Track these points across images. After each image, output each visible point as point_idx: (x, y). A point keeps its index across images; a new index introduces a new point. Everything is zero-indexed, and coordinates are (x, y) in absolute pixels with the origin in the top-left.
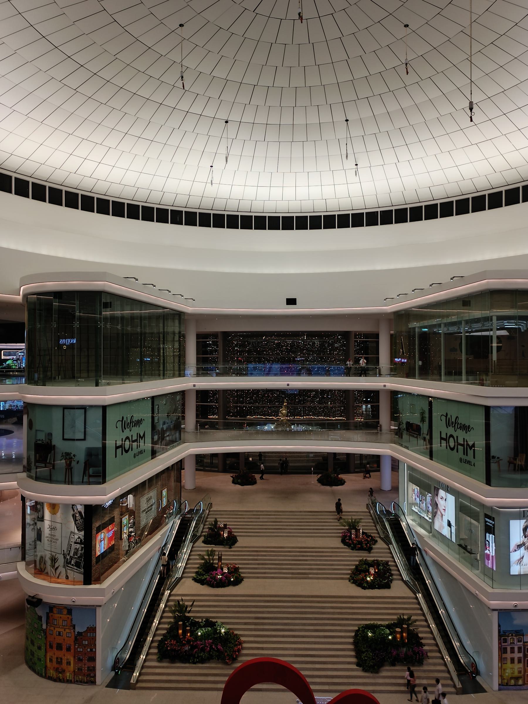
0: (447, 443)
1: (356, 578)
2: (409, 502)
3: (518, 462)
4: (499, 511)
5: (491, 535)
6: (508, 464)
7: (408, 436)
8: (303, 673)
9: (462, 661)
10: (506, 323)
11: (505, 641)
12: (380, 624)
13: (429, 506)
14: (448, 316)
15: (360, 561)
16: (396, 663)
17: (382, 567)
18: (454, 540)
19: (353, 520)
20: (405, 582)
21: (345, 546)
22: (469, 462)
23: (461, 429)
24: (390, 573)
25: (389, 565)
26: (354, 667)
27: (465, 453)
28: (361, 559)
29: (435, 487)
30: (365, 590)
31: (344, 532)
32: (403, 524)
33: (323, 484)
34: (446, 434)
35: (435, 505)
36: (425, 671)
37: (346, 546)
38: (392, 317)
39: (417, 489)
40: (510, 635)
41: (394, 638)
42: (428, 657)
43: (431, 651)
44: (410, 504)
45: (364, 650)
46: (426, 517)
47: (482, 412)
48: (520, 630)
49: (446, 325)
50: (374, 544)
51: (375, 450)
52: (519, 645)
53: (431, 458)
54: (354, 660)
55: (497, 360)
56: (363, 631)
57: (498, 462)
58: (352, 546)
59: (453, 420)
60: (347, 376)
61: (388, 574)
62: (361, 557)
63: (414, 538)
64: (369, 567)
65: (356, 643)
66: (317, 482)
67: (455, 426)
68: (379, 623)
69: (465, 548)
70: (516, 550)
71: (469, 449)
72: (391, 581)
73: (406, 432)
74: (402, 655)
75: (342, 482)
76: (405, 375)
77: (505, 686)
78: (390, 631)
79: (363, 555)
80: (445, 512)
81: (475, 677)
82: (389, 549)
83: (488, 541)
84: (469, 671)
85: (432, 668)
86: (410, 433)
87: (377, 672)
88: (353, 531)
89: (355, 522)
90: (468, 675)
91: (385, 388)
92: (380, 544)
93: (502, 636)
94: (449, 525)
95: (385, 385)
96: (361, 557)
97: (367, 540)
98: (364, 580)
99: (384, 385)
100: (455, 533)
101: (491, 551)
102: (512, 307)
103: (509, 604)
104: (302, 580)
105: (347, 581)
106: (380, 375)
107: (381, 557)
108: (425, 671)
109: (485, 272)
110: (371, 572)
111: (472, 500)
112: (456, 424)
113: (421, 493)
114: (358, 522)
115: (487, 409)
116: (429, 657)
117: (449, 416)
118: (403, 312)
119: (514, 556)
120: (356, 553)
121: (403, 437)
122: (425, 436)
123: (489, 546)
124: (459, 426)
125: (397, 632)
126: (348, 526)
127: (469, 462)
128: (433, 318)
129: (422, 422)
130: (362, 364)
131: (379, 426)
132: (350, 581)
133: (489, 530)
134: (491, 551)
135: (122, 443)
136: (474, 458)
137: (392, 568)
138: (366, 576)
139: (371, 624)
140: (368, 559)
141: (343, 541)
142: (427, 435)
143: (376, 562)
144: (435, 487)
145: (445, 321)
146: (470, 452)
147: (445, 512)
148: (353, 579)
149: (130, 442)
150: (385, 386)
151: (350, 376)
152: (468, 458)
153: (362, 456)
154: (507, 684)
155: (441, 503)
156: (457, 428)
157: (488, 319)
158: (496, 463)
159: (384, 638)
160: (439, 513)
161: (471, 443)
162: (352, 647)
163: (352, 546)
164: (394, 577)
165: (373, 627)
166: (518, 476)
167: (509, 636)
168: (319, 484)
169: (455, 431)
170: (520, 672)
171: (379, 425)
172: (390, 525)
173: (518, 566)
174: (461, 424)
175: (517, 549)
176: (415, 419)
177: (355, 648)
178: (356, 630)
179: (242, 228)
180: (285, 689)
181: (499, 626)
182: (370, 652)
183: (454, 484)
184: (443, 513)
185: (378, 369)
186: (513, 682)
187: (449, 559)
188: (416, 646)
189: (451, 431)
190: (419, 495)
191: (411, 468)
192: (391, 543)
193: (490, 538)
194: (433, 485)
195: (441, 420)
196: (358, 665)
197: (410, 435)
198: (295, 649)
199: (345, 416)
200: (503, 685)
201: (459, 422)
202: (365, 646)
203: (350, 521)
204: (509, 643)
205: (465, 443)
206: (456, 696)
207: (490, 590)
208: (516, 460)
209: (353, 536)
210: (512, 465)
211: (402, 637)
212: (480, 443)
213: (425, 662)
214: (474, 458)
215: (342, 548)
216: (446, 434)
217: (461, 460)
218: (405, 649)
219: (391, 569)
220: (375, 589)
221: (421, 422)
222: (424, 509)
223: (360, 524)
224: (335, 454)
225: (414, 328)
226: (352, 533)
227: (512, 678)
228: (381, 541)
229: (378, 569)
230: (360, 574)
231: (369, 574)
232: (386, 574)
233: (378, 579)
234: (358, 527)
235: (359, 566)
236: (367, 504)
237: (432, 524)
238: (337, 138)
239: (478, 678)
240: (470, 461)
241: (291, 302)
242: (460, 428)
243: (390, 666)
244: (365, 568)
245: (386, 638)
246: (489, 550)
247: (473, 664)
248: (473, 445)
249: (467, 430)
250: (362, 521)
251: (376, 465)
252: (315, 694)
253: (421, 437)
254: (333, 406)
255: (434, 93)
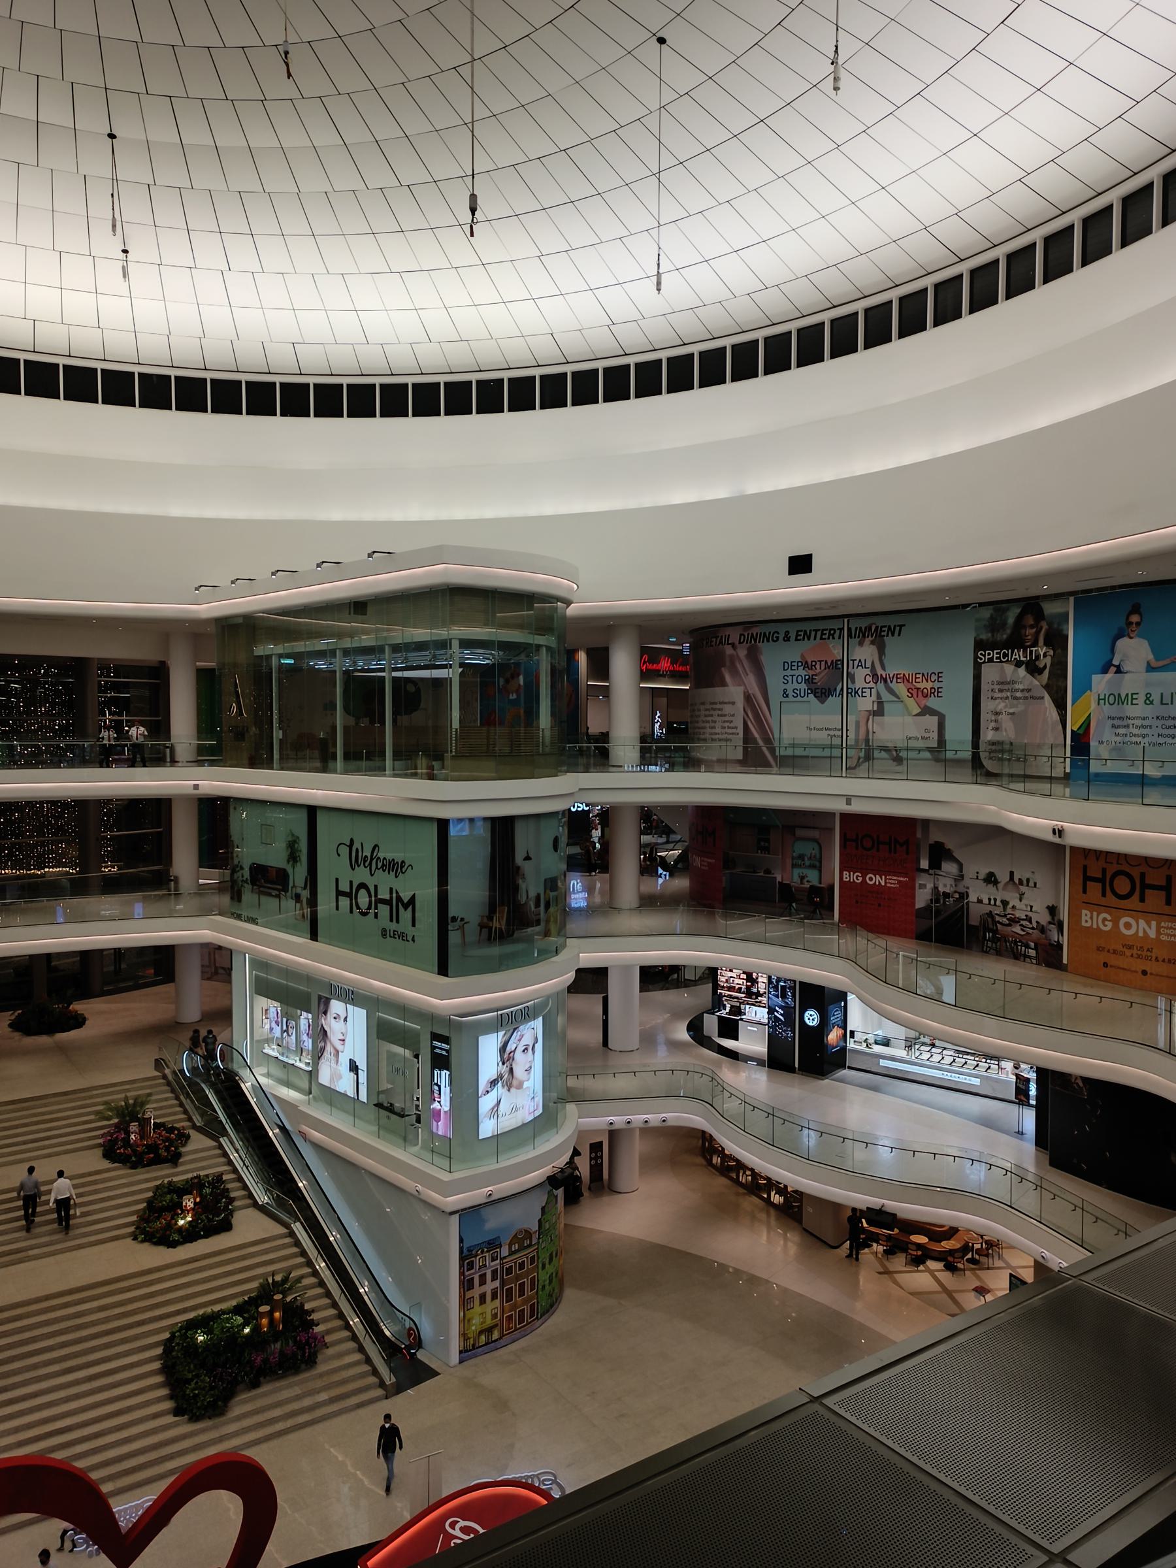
0: (351, 900)
1: (150, 1228)
2: (256, 1038)
3: (495, 924)
4: (461, 1021)
5: (443, 1072)
6: (479, 928)
7: (256, 896)
8: (80, 1464)
9: (387, 1333)
10: (468, 654)
11: (471, 1266)
12: (219, 1311)
13: (305, 1037)
14: (352, 634)
15: (157, 1187)
16: (262, 1379)
17: (208, 1191)
18: (363, 1097)
19: (131, 1102)
20: (262, 1209)
21: (114, 1165)
22: (402, 936)
23: (384, 871)
24: (228, 1197)
25: (224, 1182)
26: (171, 1419)
27: (395, 917)
28: (159, 1182)
29: (320, 998)
30: (175, 1248)
31: (109, 1132)
32: (246, 1087)
33: (29, 1032)
34: (351, 882)
35: (321, 1035)
36: (321, 1376)
37: (116, 1165)
38: (211, 629)
39: (274, 1007)
40: (479, 1252)
41: (256, 1330)
42: (326, 1346)
43: (328, 1332)
44: (258, 1041)
45: (190, 1376)
46: (298, 1064)
47: (433, 831)
48: (495, 1239)
49: (346, 652)
50: (184, 1145)
51: (174, 935)
52: (492, 1267)
53: (314, 936)
54: (168, 1405)
55: (460, 727)
56: (184, 1337)
57: (462, 928)
58: (134, 1159)
59: (368, 853)
60: (101, 767)
61: (224, 1200)
62: (156, 1179)
63: (274, 1109)
64: (180, 1197)
65: (169, 1369)
66: (10, 1030)
67: (370, 864)
68: (217, 1308)
69: (390, 1109)
70: (488, 1092)
71: (401, 909)
72: (231, 1213)
73: (250, 886)
74: (274, 1358)
75: (78, 1021)
76: (246, 761)
77: (470, 1350)
78: (244, 1318)
79: (162, 1174)
80: (343, 1045)
81: (415, 1353)
82: (221, 1147)
83: (437, 1084)
84: (403, 1346)
85: (336, 1364)
86: (261, 889)
87: (222, 1413)
88: (134, 1127)
89: (135, 1105)
90: (400, 1355)
91: (196, 792)
92: (198, 1142)
93: (466, 1258)
94: (354, 1067)
95: (198, 785)
96: (156, 1179)
97: (168, 1139)
98: (170, 1226)
99: (194, 785)
100: (366, 1084)
101: (444, 1103)
102: (486, 625)
103: (477, 1195)
104: (10, 1268)
105: (129, 1241)
106: (173, 762)
107: (203, 1168)
108: (321, 1376)
109: (440, 548)
110: (186, 1206)
111: (403, 1009)
112: (374, 861)
113: (286, 1014)
114: (143, 1104)
115: (443, 825)
116: (328, 1345)
117: (357, 845)
118: (240, 621)
119: (486, 1103)
120: (142, 1174)
121: (244, 898)
122: (299, 891)
123: (440, 1094)
124: (380, 865)
125: (262, 1315)
126: (117, 1118)
127: (402, 936)
128: (316, 638)
129: (291, 863)
130: (135, 738)
131: (172, 880)
132: (135, 1239)
133: (441, 1062)
134: (444, 1103)
136: (414, 925)
137: (229, 1186)
138: (175, 1217)
139: (199, 1315)
140: (175, 1179)
141: (110, 1153)
142: (305, 888)
143: (196, 1181)
144: (320, 998)
145: (347, 643)
146: (406, 915)
147: (343, 1045)
148: (143, 1232)
150: (196, 787)
151: (147, 764)
152: (400, 928)
153: (118, 954)
154: (474, 1347)
155: (334, 1028)
156: (377, 868)
157: (444, 644)
158: (458, 929)
159: (233, 1337)
160: (329, 1048)
161: (406, 897)
162: (159, 1379)
163: (134, 1159)
164: (237, 1203)
165: (203, 1323)
166: (495, 950)
167: (478, 1255)
168: (17, 1035)
169: (372, 875)
170: (494, 1316)
171: (172, 878)
172: (217, 1093)
173: (493, 1121)
174: (384, 859)
175: (489, 1089)
176: (275, 857)
177: (167, 1378)
178: (168, 1340)
179: (351, 415)
180: (34, 1518)
181: (461, 1240)
182: (205, 1376)
183: (371, 985)
184: (340, 1047)
185: (168, 750)
186: (483, 1338)
187: (358, 1136)
188: (302, 1331)
189: (362, 875)
190: (280, 1019)
191: (260, 964)
192: (224, 1133)
193: (443, 1076)
194: (315, 993)
195: (339, 855)
196: (177, 1412)
197: (260, 893)
198: (17, 1430)
199: (69, 863)
200: (466, 1351)
201: (381, 855)
202: (192, 1366)
203: (123, 1103)
204: (478, 1267)
205: (394, 895)
206: (386, 1401)
207: (445, 1177)
208: (490, 918)
209: (133, 1136)
210: (485, 931)
211: (272, 1321)
212: (426, 892)
213: (320, 1357)
214: (414, 925)
215: (108, 1170)
216: (351, 882)
217: (384, 933)
218: (278, 1345)
219: (228, 1189)
220: (199, 1241)
221: (288, 862)
222: (293, 1047)
223: (148, 1106)
224: (48, 957)
225: (269, 657)
226: (131, 1130)
227: (481, 1333)
228: (197, 1133)
229: (201, 1196)
230: (158, 1218)
231: (183, 1211)
232: (220, 1202)
233: (203, 1217)
234: (144, 1114)
235: (156, 1199)
236: (156, 1060)
237: (313, 1075)
238: (82, 171)
239: (421, 1355)
242: (382, 867)
243: (250, 1390)
244: (171, 1200)
245: (239, 1333)
246: (439, 1102)
247: (411, 1329)
248: (412, 900)
249: (399, 870)
250: (154, 1098)
251: (152, 971)
252: (111, 1501)
253: (289, 894)
254: (37, 842)
255: (325, 137)
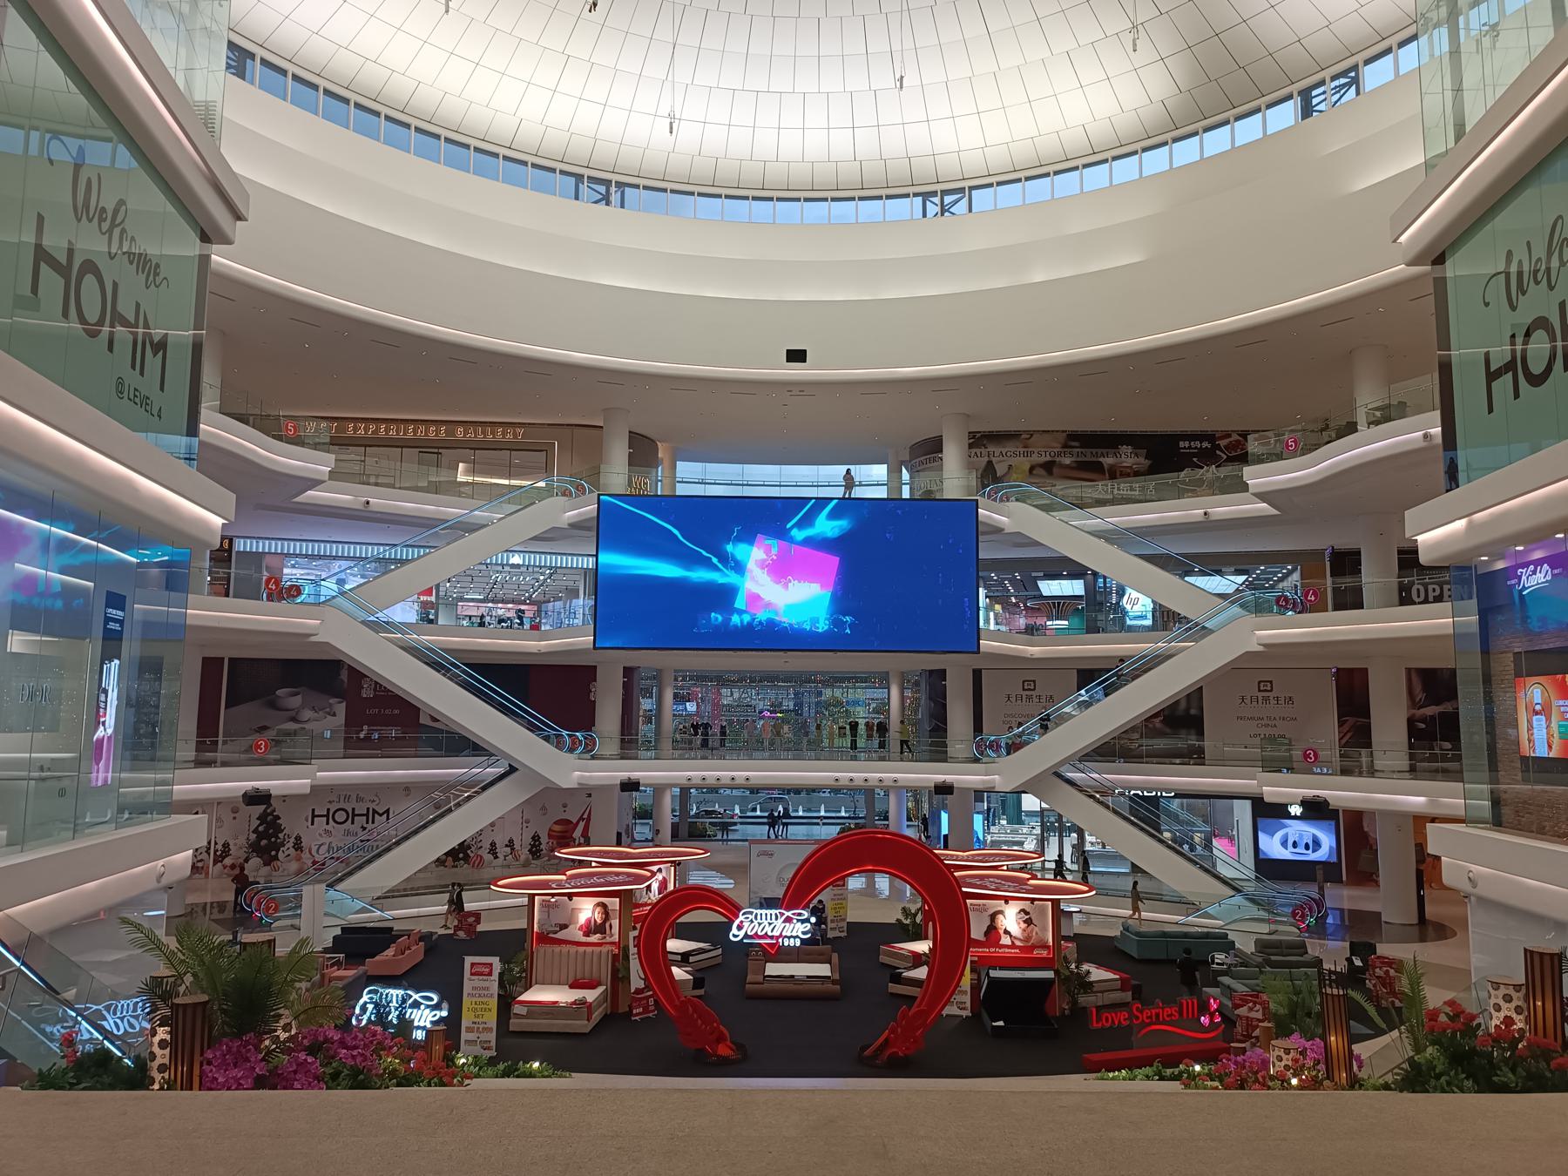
27: (137, 363)
135: (1514, 352)
146: (154, 363)
149: (1553, 339)
240: (148, 398)
241: (796, 356)
